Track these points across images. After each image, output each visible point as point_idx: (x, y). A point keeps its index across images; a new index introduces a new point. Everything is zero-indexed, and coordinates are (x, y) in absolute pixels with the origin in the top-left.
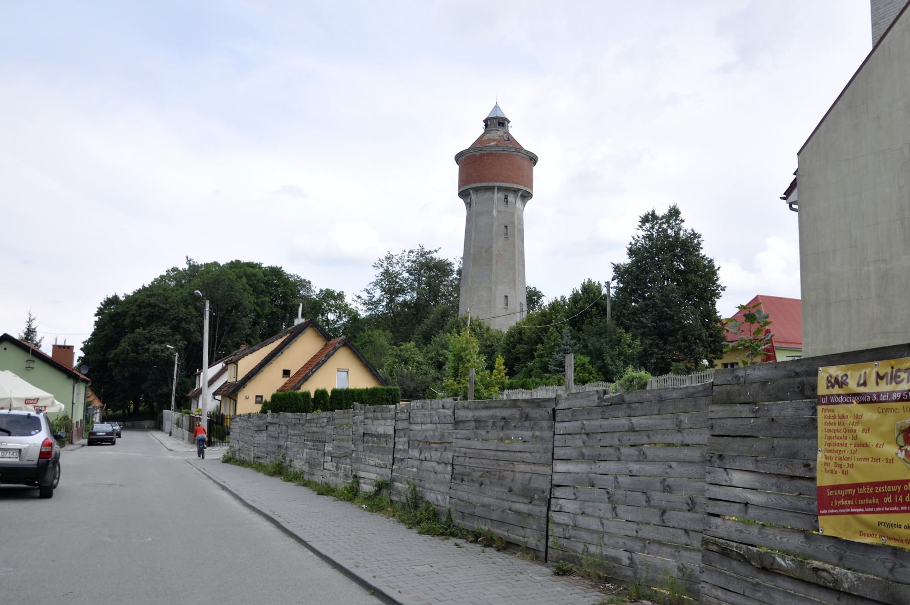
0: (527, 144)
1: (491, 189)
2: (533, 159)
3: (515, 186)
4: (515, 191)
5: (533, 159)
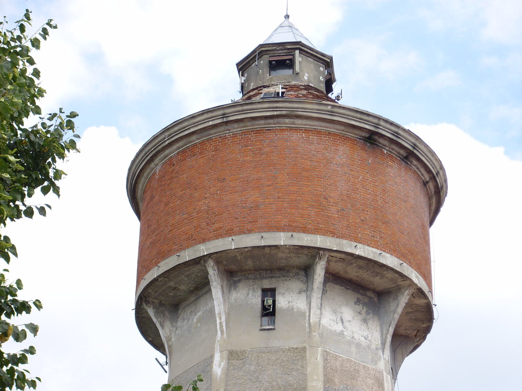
4: (299, 265)
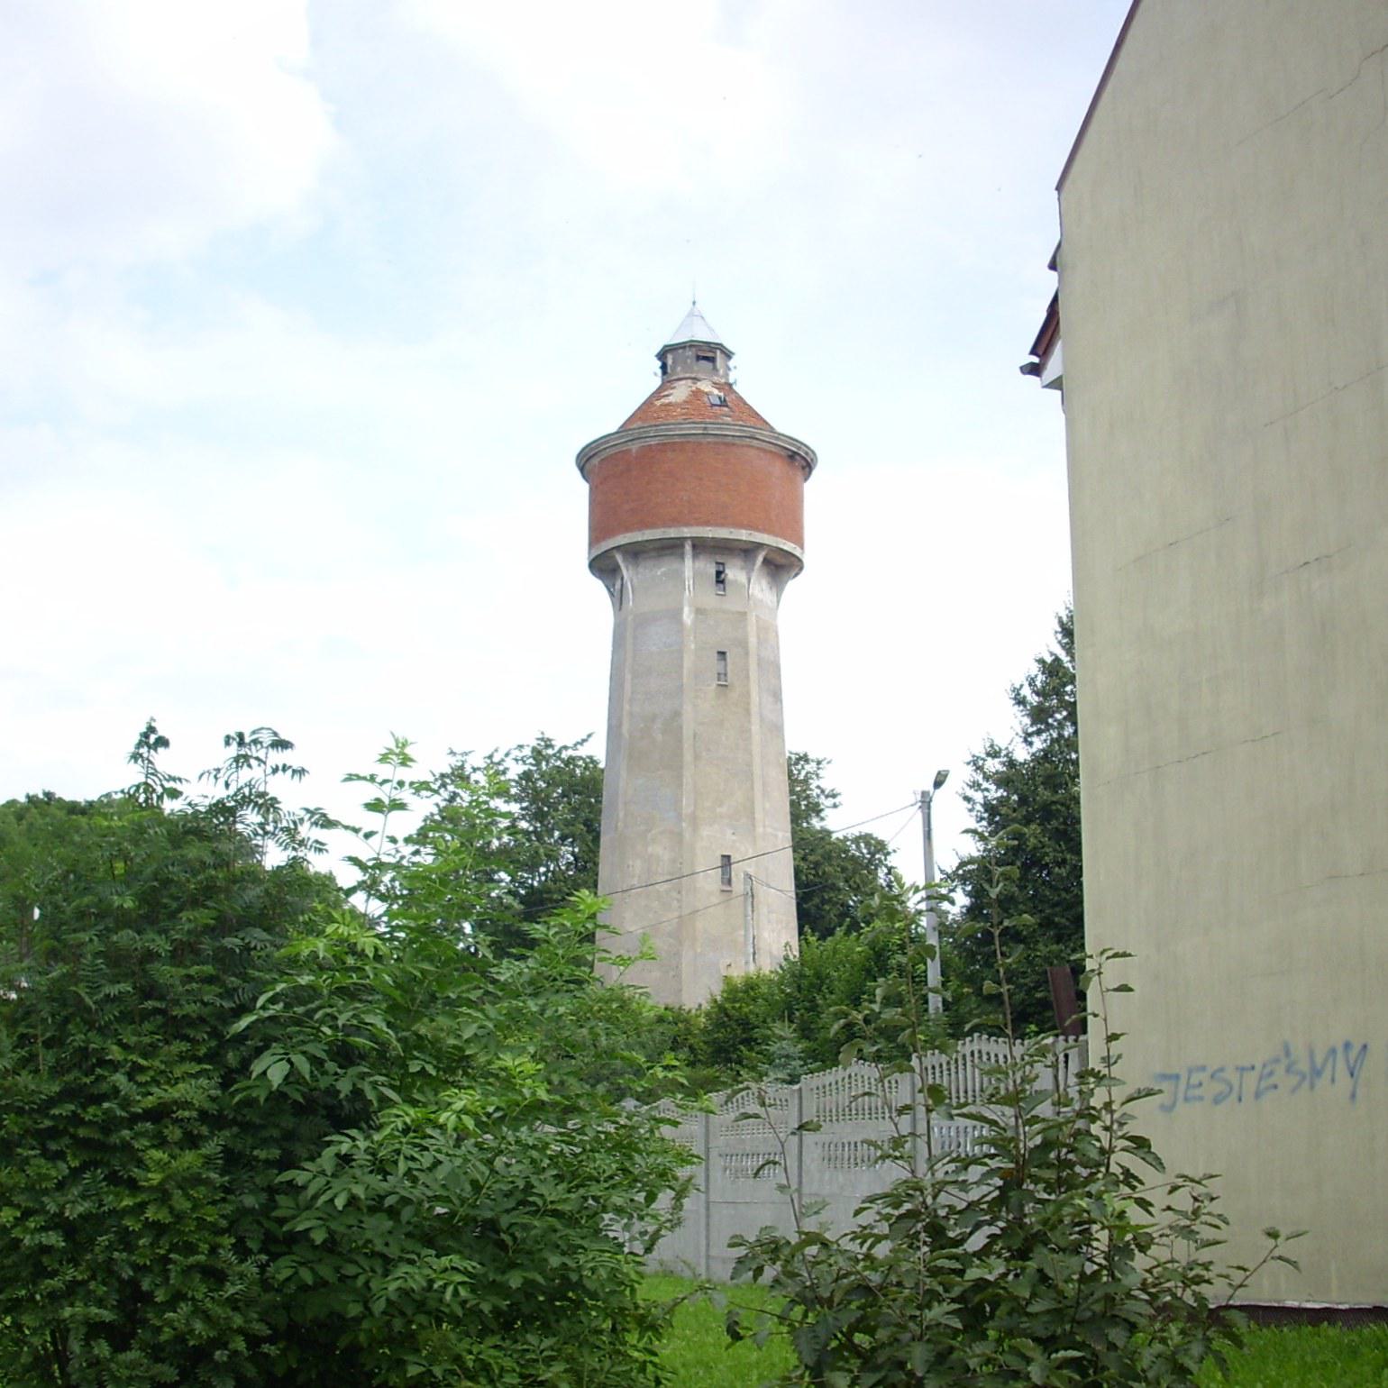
0: (786, 417)
1: (671, 548)
2: (800, 460)
3: (744, 535)
4: (747, 551)
5: (800, 460)
